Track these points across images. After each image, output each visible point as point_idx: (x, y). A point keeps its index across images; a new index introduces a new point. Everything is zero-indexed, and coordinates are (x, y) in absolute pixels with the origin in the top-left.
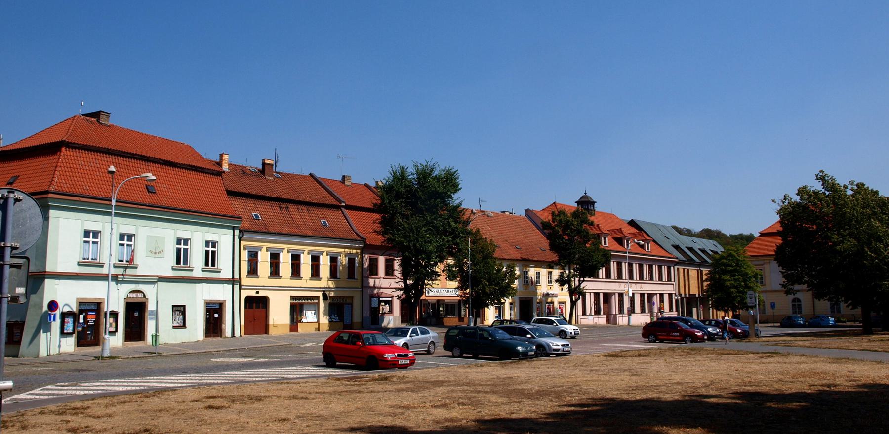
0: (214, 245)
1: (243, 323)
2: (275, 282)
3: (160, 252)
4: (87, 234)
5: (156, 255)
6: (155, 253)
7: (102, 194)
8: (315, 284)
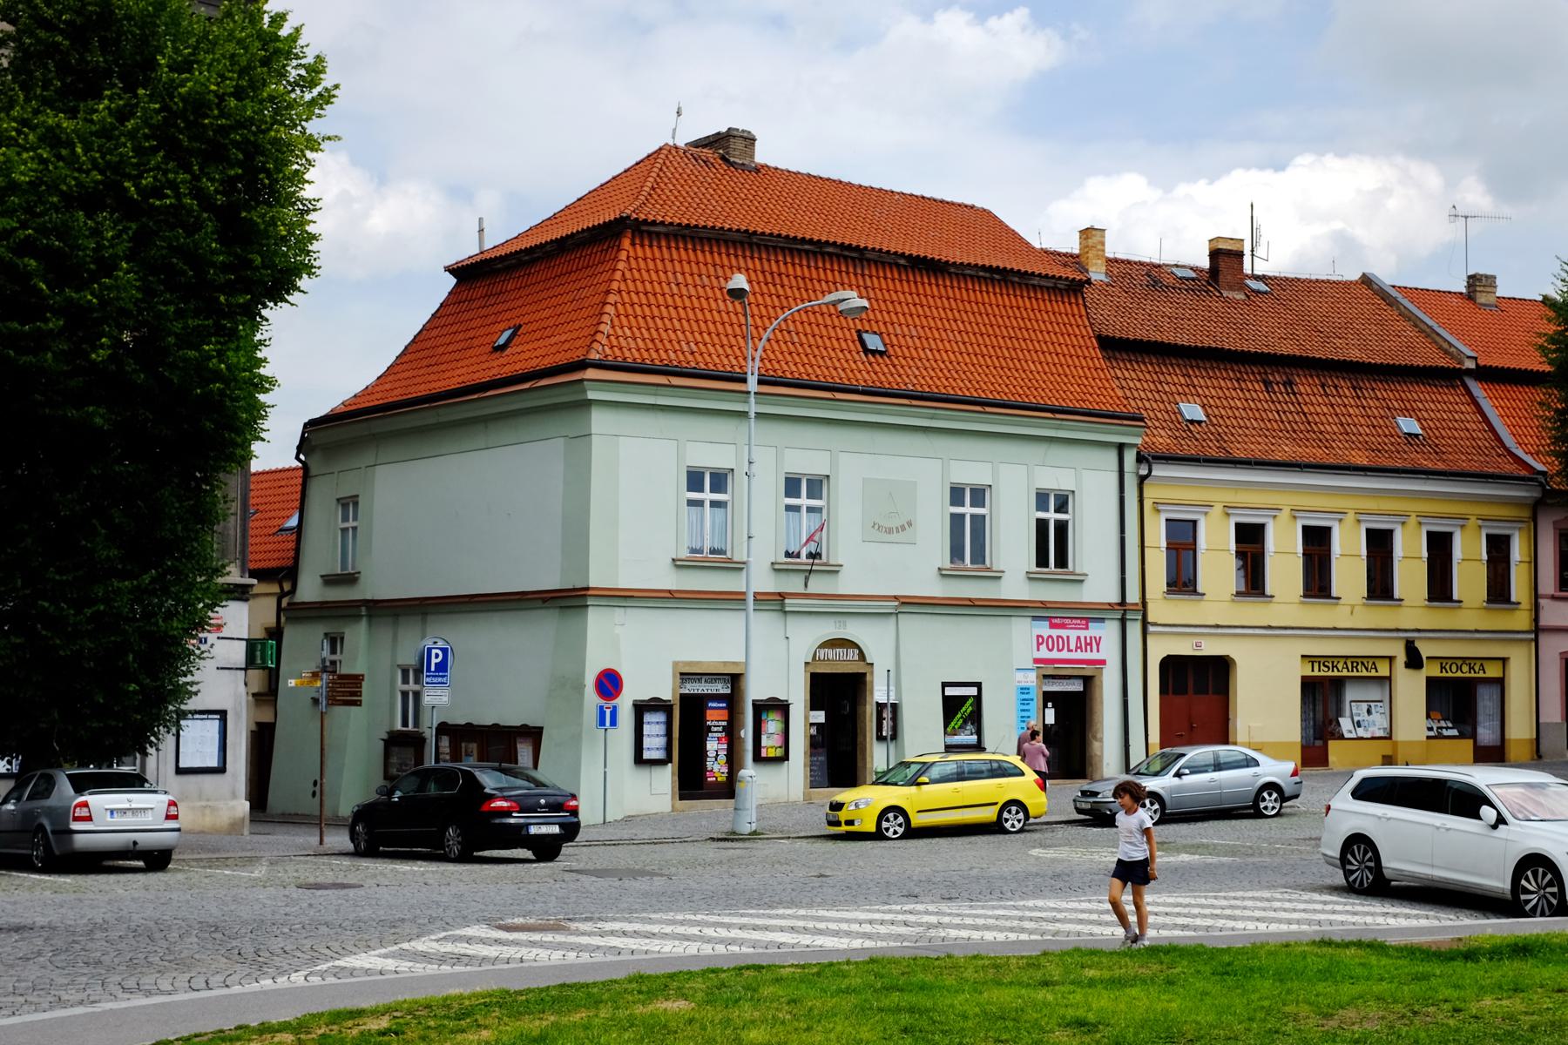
0: (979, 496)
2: (1253, 612)
3: (903, 528)
4: (695, 480)
5: (894, 537)
6: (890, 531)
7: (726, 365)
8: (1381, 615)
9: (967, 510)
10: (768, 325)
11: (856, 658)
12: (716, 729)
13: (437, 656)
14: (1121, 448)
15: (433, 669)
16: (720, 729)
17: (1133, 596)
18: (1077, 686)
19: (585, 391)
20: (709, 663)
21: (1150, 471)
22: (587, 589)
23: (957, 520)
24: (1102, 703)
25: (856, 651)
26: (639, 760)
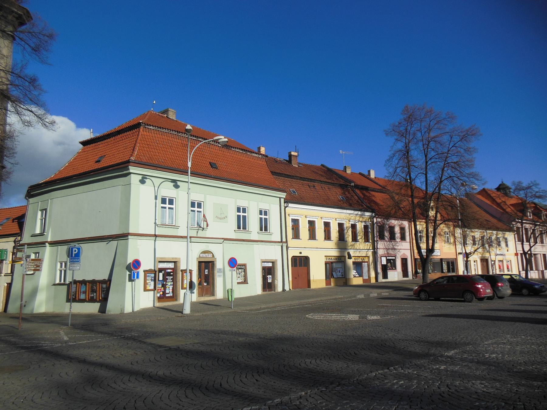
1: (291, 279)
9: (241, 214)
10: (198, 143)
11: (211, 256)
12: (169, 279)
13: (75, 251)
14: (280, 198)
15: (73, 256)
16: (171, 279)
17: (284, 240)
18: (270, 265)
19: (128, 169)
20: (169, 258)
21: (288, 205)
22: (129, 233)
23: (239, 217)
24: (277, 269)
25: (212, 254)
26: (145, 290)
